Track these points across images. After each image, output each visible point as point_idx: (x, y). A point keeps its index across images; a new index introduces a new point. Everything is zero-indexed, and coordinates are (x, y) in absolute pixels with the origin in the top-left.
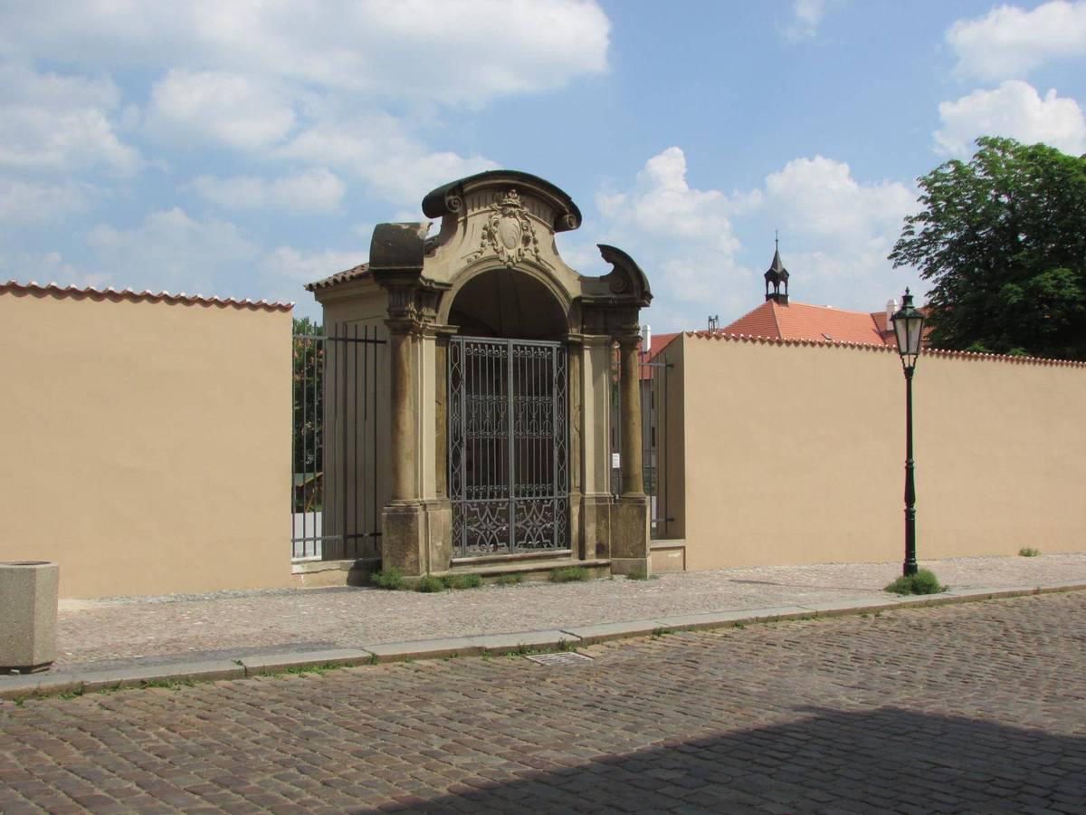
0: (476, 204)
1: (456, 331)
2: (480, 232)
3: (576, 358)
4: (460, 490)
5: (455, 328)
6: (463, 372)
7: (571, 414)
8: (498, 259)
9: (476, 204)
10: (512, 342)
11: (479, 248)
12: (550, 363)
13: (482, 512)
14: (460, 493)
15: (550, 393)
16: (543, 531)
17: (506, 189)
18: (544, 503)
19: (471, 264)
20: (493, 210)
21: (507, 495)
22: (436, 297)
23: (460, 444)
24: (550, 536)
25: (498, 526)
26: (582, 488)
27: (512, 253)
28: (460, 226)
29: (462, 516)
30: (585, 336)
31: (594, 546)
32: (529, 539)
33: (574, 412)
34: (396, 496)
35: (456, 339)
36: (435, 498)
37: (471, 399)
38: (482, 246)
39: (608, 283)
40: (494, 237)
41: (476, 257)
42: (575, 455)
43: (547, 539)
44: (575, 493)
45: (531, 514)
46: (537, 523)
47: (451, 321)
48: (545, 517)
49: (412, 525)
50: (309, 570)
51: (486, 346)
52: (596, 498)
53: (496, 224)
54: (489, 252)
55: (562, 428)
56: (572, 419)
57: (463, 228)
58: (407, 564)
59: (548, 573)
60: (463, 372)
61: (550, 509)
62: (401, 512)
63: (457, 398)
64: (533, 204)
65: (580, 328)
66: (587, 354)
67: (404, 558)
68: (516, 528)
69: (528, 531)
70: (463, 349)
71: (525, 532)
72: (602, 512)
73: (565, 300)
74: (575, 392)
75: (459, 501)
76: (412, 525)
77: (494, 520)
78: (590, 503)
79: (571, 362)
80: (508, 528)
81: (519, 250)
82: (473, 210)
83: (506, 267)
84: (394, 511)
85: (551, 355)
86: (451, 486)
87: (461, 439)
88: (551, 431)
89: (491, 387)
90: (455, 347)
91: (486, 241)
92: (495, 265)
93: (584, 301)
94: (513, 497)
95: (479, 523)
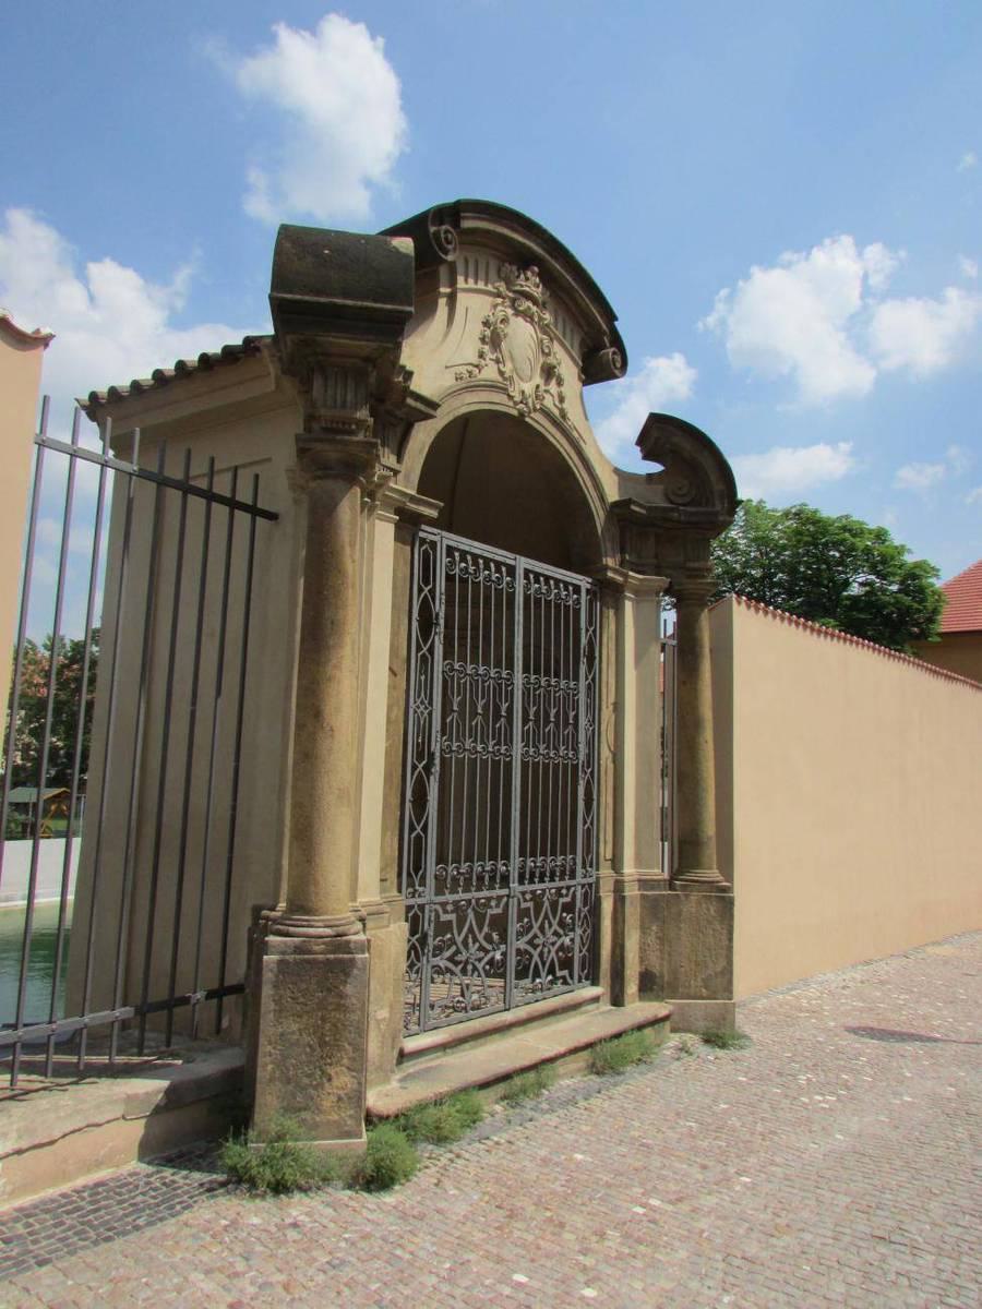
0: (482, 274)
1: (434, 513)
2: (476, 329)
3: (611, 613)
4: (423, 877)
5: (431, 505)
6: (439, 608)
7: (603, 717)
8: (504, 390)
9: (482, 274)
10: (523, 563)
11: (475, 360)
12: (577, 612)
13: (461, 921)
14: (423, 884)
15: (576, 678)
16: (557, 952)
17: (524, 260)
18: (561, 896)
19: (462, 384)
20: (499, 295)
21: (505, 880)
22: (399, 430)
23: (427, 769)
24: (567, 963)
25: (487, 952)
26: (616, 863)
27: (528, 388)
28: (442, 302)
29: (425, 936)
30: (631, 573)
31: (637, 976)
32: (537, 974)
33: (607, 714)
34: (302, 906)
35: (428, 533)
36: (377, 898)
37: (452, 670)
38: (481, 355)
39: (661, 487)
40: (499, 346)
41: (470, 372)
42: (607, 798)
43: (563, 968)
44: (606, 871)
45: (541, 919)
46: (552, 940)
47: (425, 486)
48: (562, 924)
49: (349, 989)
50: (24, 1144)
51: (571, 588)
52: (639, 881)
53: (505, 321)
54: (490, 373)
55: (590, 744)
56: (603, 727)
57: (446, 309)
58: (327, 1103)
59: (585, 1054)
60: (439, 608)
61: (569, 908)
62: (319, 952)
63: (426, 663)
64: (556, 311)
65: (618, 557)
66: (628, 605)
67: (320, 1086)
68: (518, 951)
69: (536, 954)
70: (442, 560)
71: (531, 956)
72: (654, 909)
73: (598, 503)
74: (608, 676)
75: (420, 901)
76: (349, 989)
77: (480, 937)
78: (632, 891)
79: (604, 620)
80: (504, 954)
81: (538, 387)
82: (476, 283)
83: (515, 413)
84: (298, 950)
85: (578, 601)
86: (409, 865)
87: (431, 756)
88: (576, 750)
89: (475, 647)
90: (426, 552)
91: (486, 348)
92: (499, 403)
93: (633, 507)
94: (514, 885)
95: (454, 948)
